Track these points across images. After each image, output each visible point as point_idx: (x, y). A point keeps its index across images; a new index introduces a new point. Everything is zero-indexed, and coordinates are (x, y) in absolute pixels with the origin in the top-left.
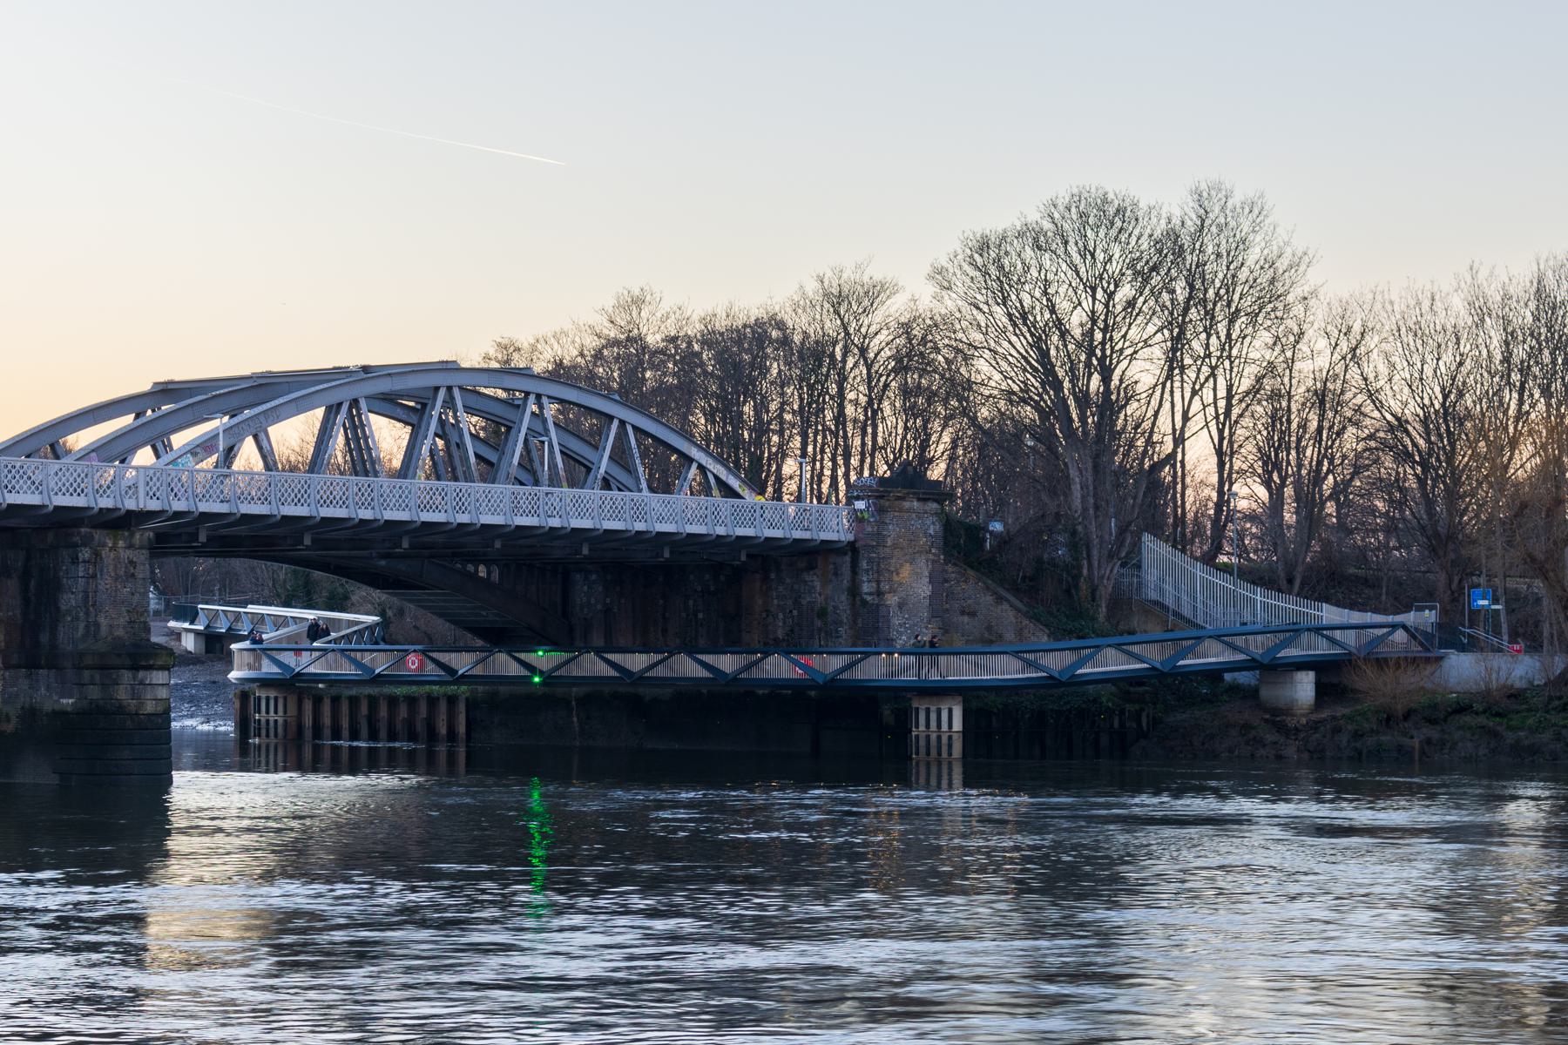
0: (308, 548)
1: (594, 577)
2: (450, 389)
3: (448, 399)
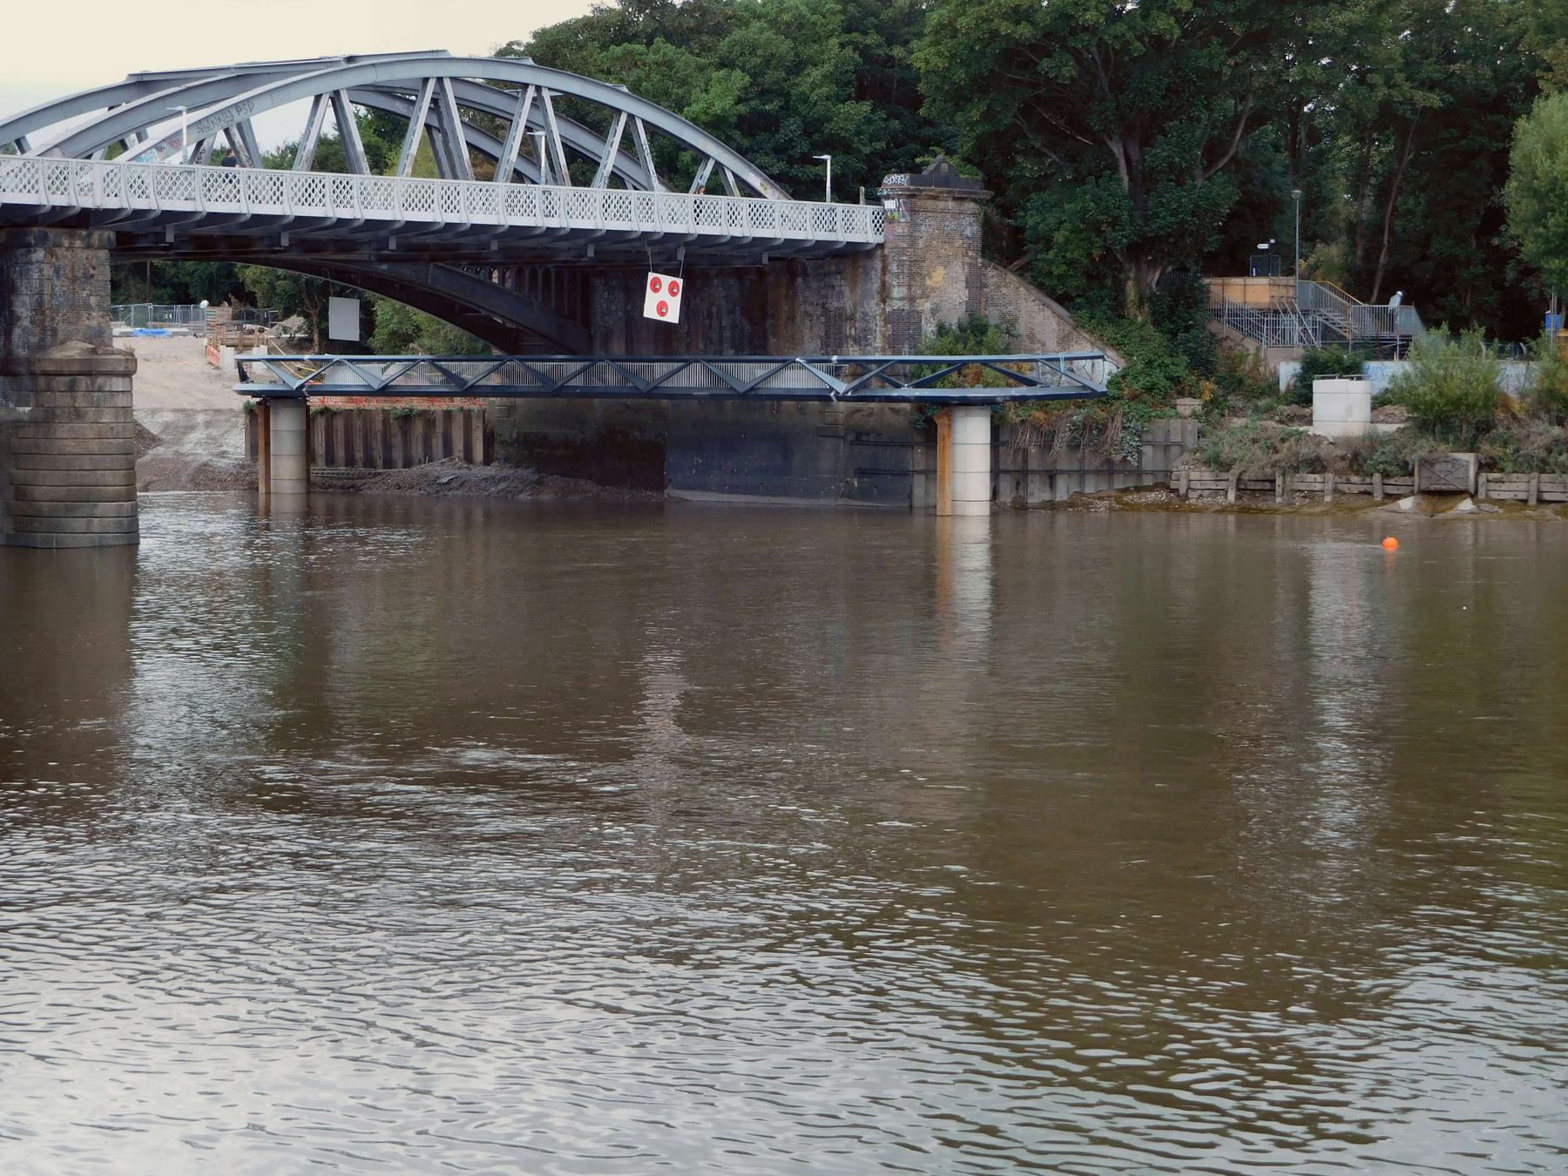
0: (286, 250)
1: (614, 283)
2: (440, 80)
3: (438, 90)
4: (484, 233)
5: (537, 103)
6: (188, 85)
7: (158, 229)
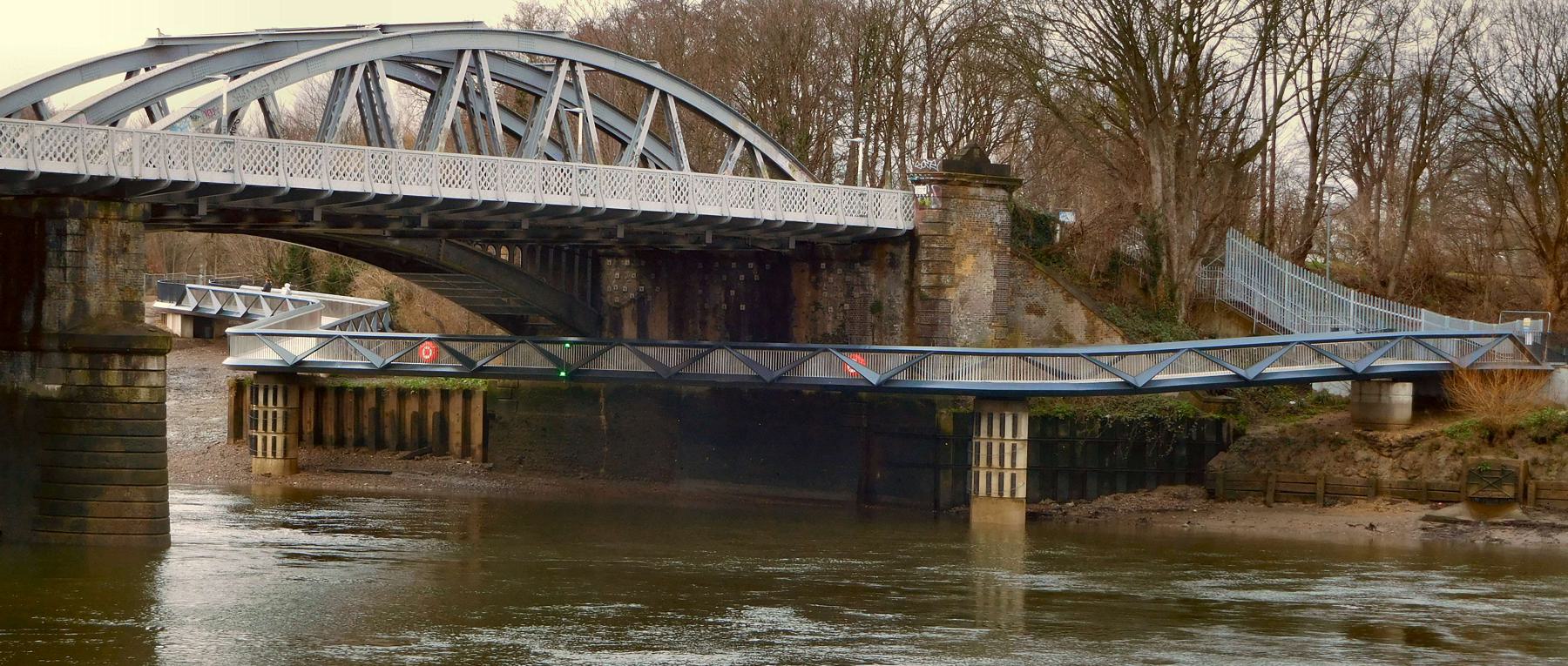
2: (475, 52)
3: (473, 64)
4: (267, 195)
5: (572, 84)
6: (215, 52)
7: (191, 201)
